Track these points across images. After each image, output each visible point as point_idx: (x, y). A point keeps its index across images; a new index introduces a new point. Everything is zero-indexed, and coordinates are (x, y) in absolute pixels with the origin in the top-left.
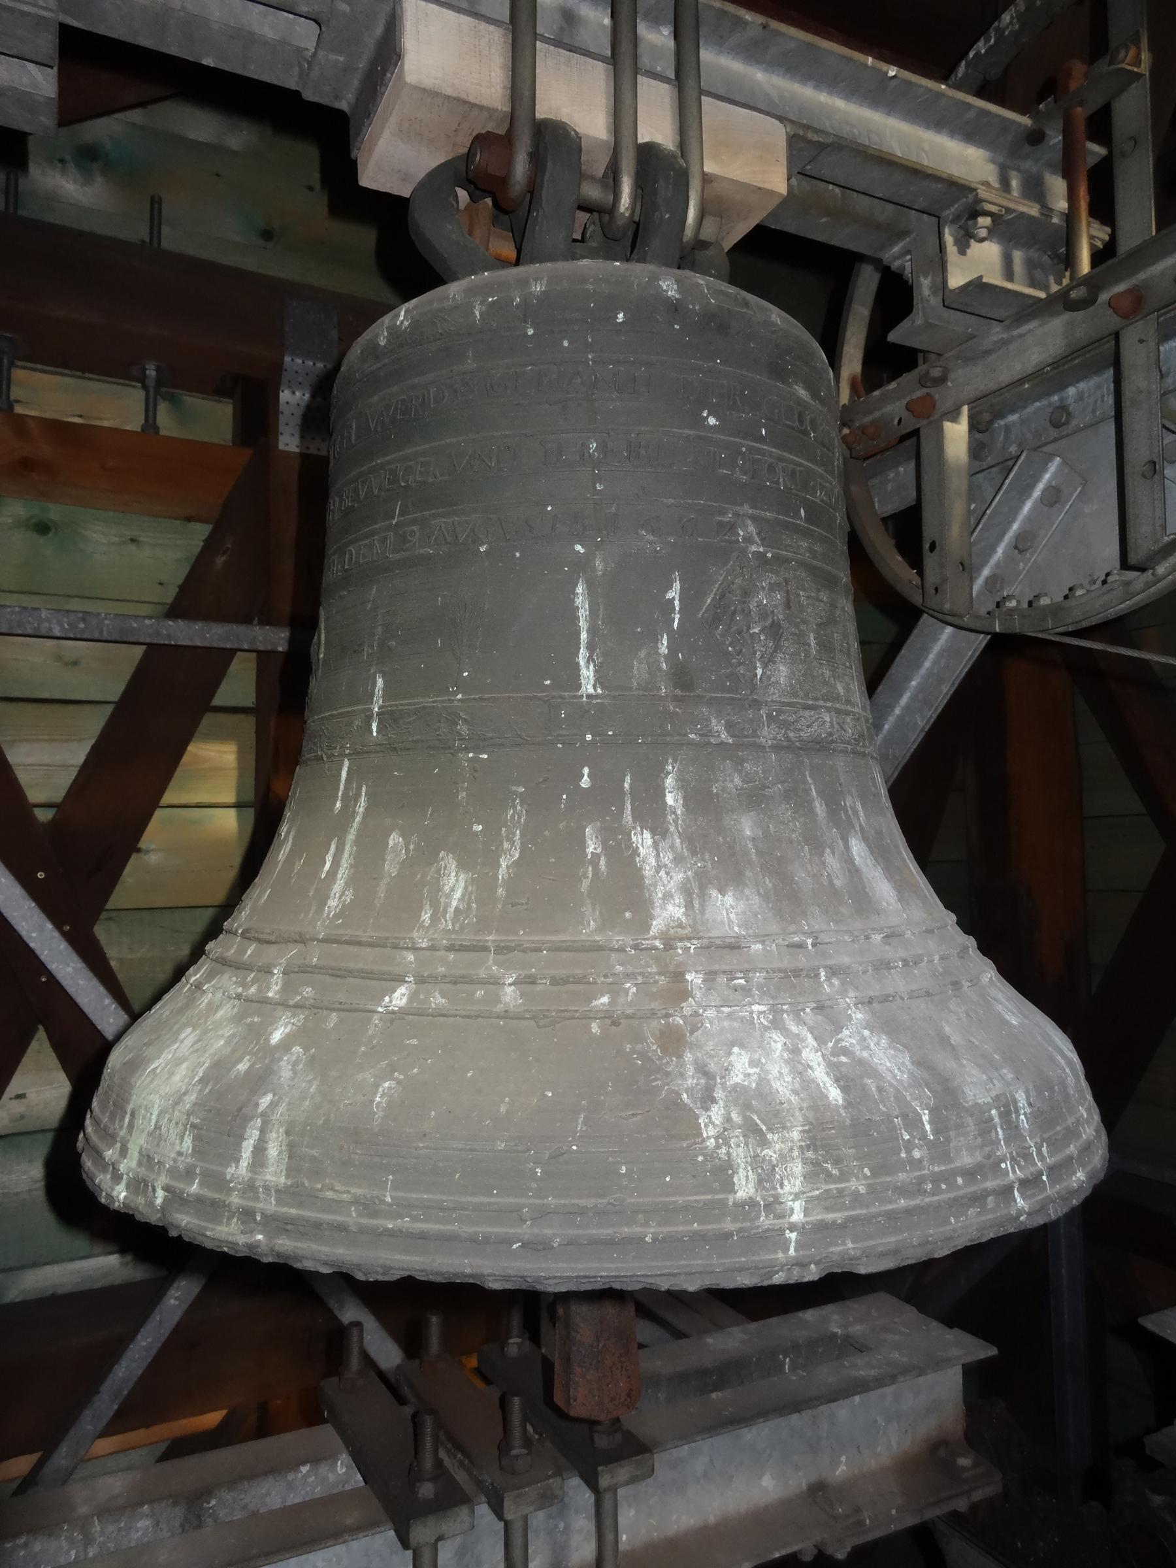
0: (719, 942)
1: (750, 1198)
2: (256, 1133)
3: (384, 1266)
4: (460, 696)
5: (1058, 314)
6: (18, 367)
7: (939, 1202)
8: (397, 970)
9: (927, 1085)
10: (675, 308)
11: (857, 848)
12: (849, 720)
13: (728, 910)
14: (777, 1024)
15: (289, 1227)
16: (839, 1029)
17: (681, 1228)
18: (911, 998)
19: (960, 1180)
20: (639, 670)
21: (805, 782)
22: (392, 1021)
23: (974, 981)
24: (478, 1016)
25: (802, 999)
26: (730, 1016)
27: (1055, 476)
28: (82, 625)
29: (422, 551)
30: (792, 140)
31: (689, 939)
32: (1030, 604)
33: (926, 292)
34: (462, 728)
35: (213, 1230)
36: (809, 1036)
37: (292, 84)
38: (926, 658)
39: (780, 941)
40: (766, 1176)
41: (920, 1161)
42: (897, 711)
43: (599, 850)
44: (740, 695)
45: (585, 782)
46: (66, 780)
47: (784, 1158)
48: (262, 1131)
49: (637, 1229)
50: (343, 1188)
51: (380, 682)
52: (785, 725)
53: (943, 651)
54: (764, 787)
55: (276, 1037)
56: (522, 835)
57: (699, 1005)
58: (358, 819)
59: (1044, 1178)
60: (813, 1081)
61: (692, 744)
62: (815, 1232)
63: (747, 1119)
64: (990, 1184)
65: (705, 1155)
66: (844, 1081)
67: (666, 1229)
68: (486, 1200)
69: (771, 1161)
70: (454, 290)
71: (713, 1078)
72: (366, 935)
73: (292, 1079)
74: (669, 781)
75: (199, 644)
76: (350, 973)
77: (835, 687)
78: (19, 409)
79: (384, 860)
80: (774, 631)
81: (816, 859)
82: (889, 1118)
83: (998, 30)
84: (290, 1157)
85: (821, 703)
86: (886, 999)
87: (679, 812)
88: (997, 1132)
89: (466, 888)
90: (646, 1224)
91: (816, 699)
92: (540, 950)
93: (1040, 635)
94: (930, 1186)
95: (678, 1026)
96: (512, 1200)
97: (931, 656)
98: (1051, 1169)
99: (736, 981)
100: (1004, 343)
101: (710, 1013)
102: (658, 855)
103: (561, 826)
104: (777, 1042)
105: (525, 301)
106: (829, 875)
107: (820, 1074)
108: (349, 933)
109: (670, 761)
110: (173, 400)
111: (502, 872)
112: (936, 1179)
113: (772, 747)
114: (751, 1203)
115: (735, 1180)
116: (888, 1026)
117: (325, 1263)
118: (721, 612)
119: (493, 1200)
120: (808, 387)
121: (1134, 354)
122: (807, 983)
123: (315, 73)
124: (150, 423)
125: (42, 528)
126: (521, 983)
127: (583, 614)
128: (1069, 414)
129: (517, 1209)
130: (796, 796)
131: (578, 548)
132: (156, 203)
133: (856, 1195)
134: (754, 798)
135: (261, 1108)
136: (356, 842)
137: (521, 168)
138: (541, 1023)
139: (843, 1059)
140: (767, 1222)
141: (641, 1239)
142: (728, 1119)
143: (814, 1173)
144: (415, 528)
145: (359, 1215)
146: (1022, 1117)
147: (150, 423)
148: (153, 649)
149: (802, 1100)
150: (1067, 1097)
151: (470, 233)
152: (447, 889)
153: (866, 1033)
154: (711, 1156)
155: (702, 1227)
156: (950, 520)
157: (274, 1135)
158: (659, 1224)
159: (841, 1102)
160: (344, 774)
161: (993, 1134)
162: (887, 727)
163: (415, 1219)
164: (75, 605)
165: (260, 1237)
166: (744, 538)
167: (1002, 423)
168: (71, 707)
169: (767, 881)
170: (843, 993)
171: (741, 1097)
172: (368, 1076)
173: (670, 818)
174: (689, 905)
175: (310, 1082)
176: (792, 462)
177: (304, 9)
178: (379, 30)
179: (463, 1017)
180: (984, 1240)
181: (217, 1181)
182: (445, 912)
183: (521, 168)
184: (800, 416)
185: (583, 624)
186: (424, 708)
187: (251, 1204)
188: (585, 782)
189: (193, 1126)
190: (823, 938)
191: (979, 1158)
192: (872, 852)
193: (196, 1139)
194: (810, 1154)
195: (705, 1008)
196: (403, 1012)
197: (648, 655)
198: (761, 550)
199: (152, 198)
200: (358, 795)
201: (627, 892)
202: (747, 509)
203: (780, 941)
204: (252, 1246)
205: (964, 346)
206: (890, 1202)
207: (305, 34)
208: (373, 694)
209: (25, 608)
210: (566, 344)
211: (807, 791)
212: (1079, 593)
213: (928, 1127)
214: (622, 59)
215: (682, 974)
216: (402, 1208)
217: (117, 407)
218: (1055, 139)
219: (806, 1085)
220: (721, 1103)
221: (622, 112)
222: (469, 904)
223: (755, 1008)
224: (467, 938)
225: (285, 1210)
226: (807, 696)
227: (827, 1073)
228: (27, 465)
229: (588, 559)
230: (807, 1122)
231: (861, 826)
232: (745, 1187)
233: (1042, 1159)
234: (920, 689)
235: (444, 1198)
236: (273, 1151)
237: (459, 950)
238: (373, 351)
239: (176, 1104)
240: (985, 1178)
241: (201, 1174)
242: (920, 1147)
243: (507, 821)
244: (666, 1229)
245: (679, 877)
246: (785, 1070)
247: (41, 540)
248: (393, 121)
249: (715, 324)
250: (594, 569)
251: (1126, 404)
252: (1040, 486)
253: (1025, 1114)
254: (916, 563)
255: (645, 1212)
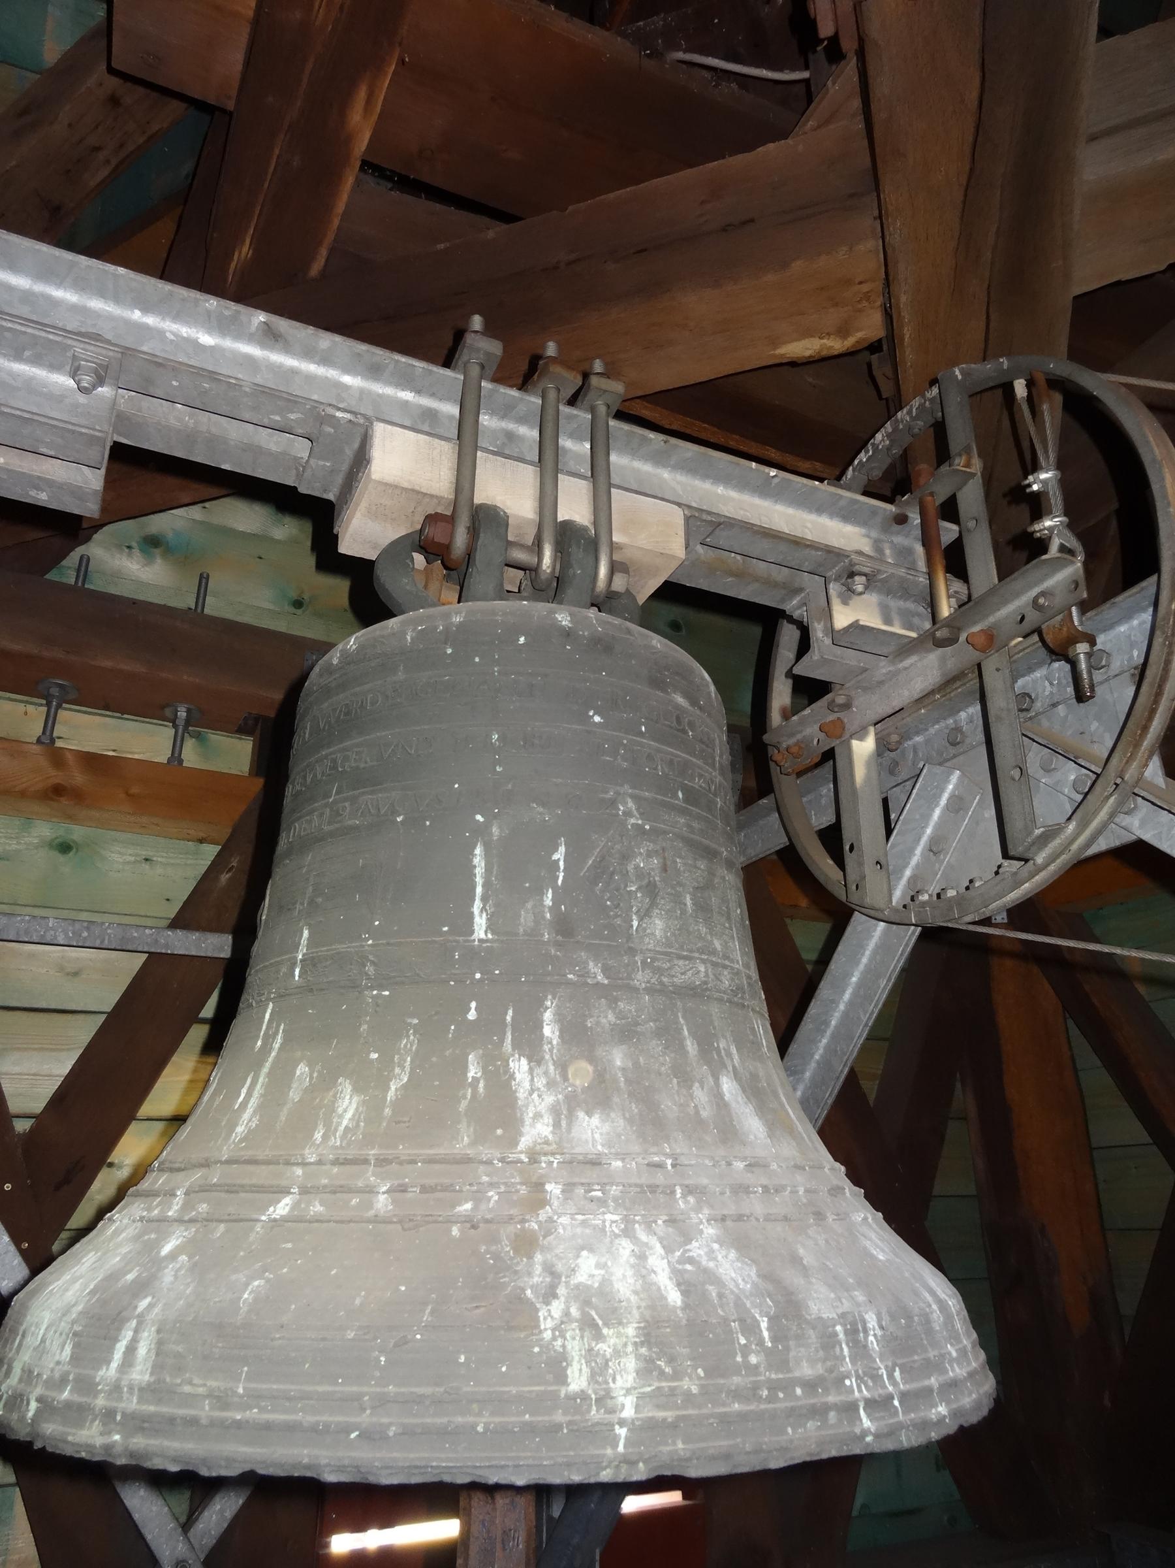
0: (581, 1157)
1: (582, 1391)
2: (130, 1334)
3: (227, 1459)
4: (370, 942)
5: (929, 651)
6: (66, 709)
7: (775, 1409)
8: (284, 1183)
9: (770, 1296)
10: (567, 634)
11: (728, 1085)
12: (726, 973)
13: (592, 1130)
14: (628, 1233)
15: (146, 1425)
16: (689, 1241)
17: (513, 1419)
18: (765, 1220)
19: (799, 1391)
20: (526, 919)
21: (677, 1023)
22: (272, 1228)
23: (842, 1217)
24: (349, 1222)
25: (655, 1212)
26: (584, 1223)
27: (956, 787)
28: (85, 934)
29: (350, 822)
30: (687, 519)
31: (553, 1154)
32: (939, 896)
33: (820, 634)
34: (370, 969)
35: (74, 1434)
36: (658, 1245)
37: (290, 482)
38: (863, 954)
39: (639, 1160)
40: (599, 1370)
41: (757, 1367)
42: (842, 1007)
43: (479, 1075)
44: (617, 943)
45: (472, 1015)
46: (49, 1088)
47: (617, 1353)
48: (136, 1331)
49: (471, 1419)
50: (201, 1382)
51: (306, 933)
52: (659, 971)
53: (878, 948)
54: (637, 1024)
55: (166, 1249)
56: (412, 1062)
57: (555, 1212)
58: (273, 1054)
59: (896, 1403)
60: (655, 1284)
61: (569, 983)
62: (644, 1429)
63: (585, 1314)
64: (832, 1399)
65: (541, 1347)
66: (686, 1286)
67: (497, 1419)
68: (330, 1388)
69: (604, 1355)
70: (392, 623)
71: (560, 1277)
72: (260, 1155)
73: (172, 1283)
74: (548, 1016)
75: (194, 953)
76: (243, 1188)
77: (711, 942)
78: (59, 744)
79: (290, 1088)
80: (651, 890)
81: (684, 1091)
82: (726, 1321)
83: (873, 444)
84: (157, 1355)
85: (697, 955)
86: (740, 1218)
87: (555, 1042)
88: (842, 1349)
89: (357, 1109)
90: (480, 1414)
91: (691, 951)
92: (414, 1162)
93: (950, 925)
94: (765, 1393)
95: (533, 1231)
96: (355, 1389)
97: (868, 953)
98: (904, 1396)
99: (593, 1193)
100: (893, 675)
101: (564, 1220)
102: (532, 1080)
103: (447, 1053)
104: (625, 1248)
105: (447, 629)
106: (696, 1106)
107: (663, 1279)
108: (248, 1154)
109: (550, 997)
110: (198, 736)
111: (391, 1095)
112: (774, 1387)
113: (645, 989)
114: (583, 1395)
115: (569, 1372)
116: (741, 1244)
117: (175, 1460)
118: (601, 871)
119: (337, 1389)
120: (687, 695)
121: (994, 681)
122: (662, 1198)
123: (308, 473)
124: (176, 758)
125: (65, 848)
126: (394, 1191)
127: (479, 871)
128: (962, 733)
129: (358, 1397)
130: (669, 1035)
131: (479, 818)
132: (204, 580)
133: (688, 1395)
134: (626, 1033)
135: (139, 1310)
136: (269, 1074)
137: (460, 540)
138: (406, 1226)
139: (688, 1267)
140: (598, 1416)
141: (474, 1427)
142: (567, 1313)
143: (647, 1369)
144: (347, 804)
145: (211, 1409)
146: (871, 1338)
147: (176, 758)
148: (155, 959)
149: (641, 1299)
150: (929, 1331)
151: (426, 587)
152: (340, 1110)
153: (716, 1246)
154: (547, 1347)
155: (533, 1419)
156: (864, 825)
157: (146, 1334)
158: (492, 1414)
159: (679, 1303)
160: (267, 1016)
161: (838, 1349)
162: (833, 1023)
163: (262, 1410)
164: (84, 916)
165: (117, 1437)
166: (624, 812)
167: (910, 743)
168: (69, 1016)
169: (634, 1106)
170: (698, 1209)
171: (583, 1296)
172: (241, 1277)
173: (546, 1047)
174: (557, 1125)
175: (188, 1284)
176: (672, 754)
177: (300, 431)
178: (356, 445)
179: (336, 1222)
180: (825, 1456)
181: (86, 1385)
182: (336, 1130)
183: (460, 540)
184: (678, 718)
185: (479, 880)
186: (338, 953)
187: (115, 1404)
188: (472, 1015)
189: (75, 1334)
190: (684, 1160)
191: (821, 1371)
192: (744, 1091)
193: (76, 1346)
194: (643, 1350)
195: (563, 1218)
196: (284, 1220)
197: (535, 906)
198: (640, 822)
199: (201, 576)
200: (276, 1033)
201: (501, 1111)
202: (627, 789)
203: (639, 1160)
204: (108, 1448)
205: (860, 677)
206: (724, 1405)
207: (301, 449)
208: (299, 944)
209: (34, 917)
210: (477, 660)
211: (679, 1031)
212: (977, 884)
213: (766, 1334)
214: (548, 462)
215: (543, 1185)
216: (254, 1398)
217: (144, 741)
218: (915, 519)
219: (649, 1290)
220: (563, 1299)
221: (547, 499)
222: (358, 1126)
223: (609, 1217)
224: (352, 1153)
225: (144, 1407)
226: (682, 948)
227: (670, 1278)
228: (57, 791)
229: (487, 825)
230: (643, 1319)
231: (734, 1067)
232: (578, 1380)
233: (894, 1383)
234: (860, 985)
235: (293, 1387)
236: (142, 1350)
237: (342, 1164)
238: (329, 670)
239: (64, 1315)
240: (826, 1391)
241: (75, 1380)
242: (757, 1353)
243: (399, 1049)
244: (497, 1419)
245: (550, 1099)
246: (630, 1273)
247: (61, 858)
248: (363, 505)
249: (602, 646)
250: (491, 834)
251: (992, 719)
252: (945, 797)
253: (875, 1335)
254: (840, 863)
255: (478, 1401)
